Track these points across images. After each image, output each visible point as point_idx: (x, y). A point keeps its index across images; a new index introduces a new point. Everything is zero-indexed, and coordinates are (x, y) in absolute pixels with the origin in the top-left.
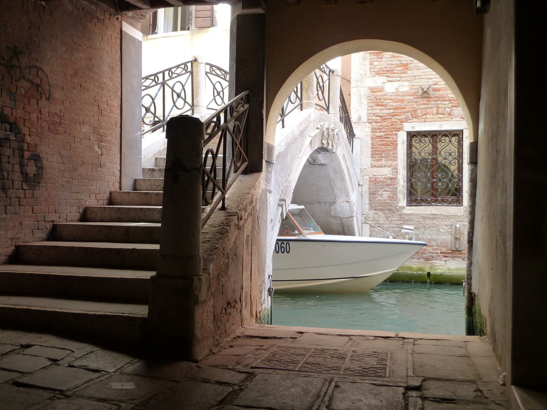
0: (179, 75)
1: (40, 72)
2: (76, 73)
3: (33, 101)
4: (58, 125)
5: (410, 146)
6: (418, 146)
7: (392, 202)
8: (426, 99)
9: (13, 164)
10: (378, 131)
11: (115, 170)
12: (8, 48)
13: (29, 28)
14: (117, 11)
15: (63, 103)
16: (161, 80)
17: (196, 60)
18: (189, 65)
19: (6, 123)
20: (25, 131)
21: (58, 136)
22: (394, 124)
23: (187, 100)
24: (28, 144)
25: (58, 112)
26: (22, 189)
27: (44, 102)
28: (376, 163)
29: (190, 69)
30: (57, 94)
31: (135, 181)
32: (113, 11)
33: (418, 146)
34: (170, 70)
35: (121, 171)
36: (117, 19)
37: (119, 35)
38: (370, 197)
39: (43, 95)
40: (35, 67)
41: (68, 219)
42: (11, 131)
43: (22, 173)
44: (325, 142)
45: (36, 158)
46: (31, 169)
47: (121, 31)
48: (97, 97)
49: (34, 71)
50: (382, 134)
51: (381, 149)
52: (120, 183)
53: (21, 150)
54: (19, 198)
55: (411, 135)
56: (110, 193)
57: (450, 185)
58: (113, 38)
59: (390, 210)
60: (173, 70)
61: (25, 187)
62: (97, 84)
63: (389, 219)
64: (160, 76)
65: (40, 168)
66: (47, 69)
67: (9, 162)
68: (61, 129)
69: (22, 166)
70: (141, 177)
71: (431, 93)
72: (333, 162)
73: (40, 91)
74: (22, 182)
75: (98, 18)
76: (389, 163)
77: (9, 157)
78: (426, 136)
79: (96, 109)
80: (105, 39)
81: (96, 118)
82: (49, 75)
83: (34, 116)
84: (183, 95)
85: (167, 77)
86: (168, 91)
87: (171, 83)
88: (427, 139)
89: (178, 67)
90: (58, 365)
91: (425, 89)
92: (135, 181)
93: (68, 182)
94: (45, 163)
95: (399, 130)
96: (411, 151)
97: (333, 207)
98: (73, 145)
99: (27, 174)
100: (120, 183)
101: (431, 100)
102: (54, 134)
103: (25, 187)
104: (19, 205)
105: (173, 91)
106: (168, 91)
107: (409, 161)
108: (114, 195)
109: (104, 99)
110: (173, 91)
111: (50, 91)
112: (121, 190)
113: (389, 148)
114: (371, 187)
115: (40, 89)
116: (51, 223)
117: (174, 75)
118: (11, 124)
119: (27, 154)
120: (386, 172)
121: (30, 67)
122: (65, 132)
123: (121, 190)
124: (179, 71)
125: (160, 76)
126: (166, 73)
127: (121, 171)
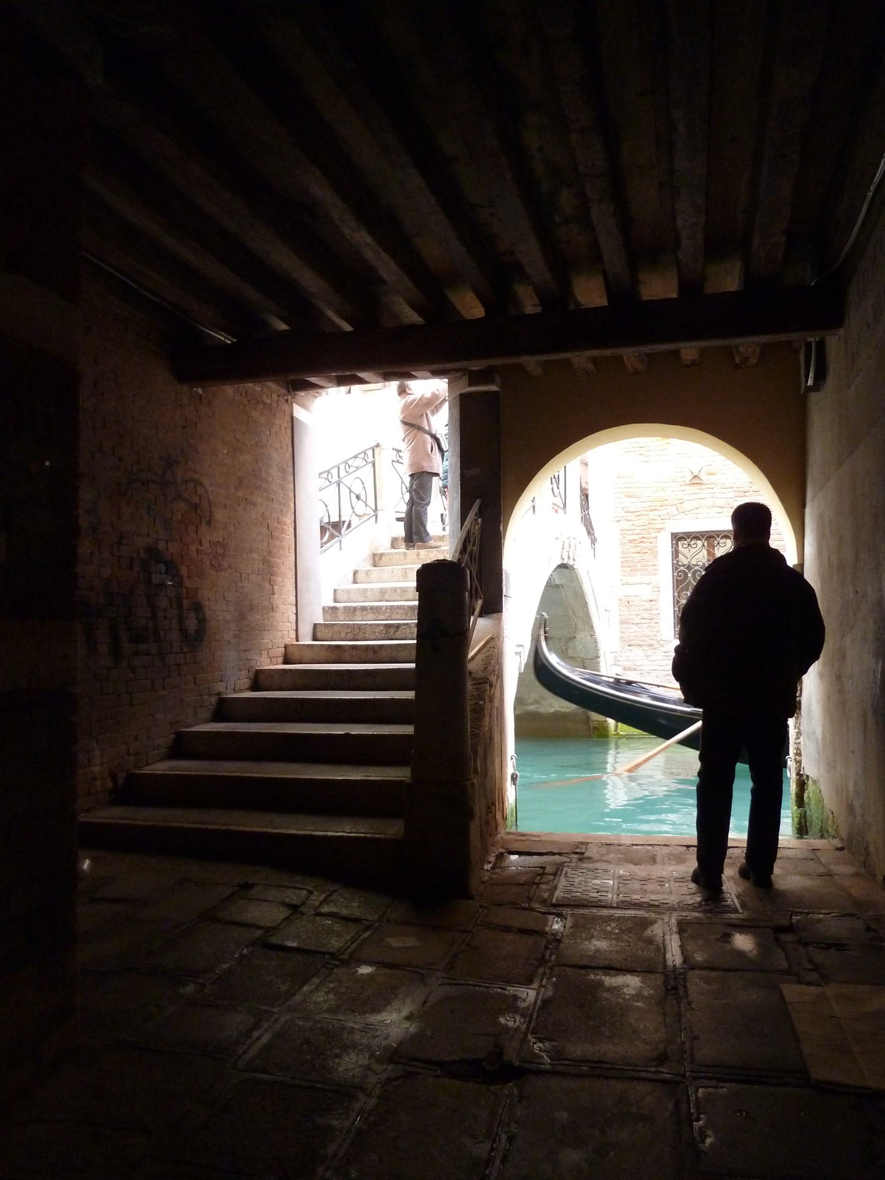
0: (358, 468)
1: (199, 487)
2: (241, 482)
3: (191, 529)
4: (220, 558)
5: (676, 553)
6: (685, 551)
7: (654, 633)
8: (697, 487)
9: (170, 619)
10: (629, 532)
11: (290, 613)
12: (160, 457)
13: (184, 427)
14: (289, 391)
15: (226, 527)
16: (336, 478)
17: (378, 446)
18: (370, 453)
19: (160, 562)
20: (184, 571)
21: (222, 573)
22: (652, 522)
23: (368, 503)
24: (187, 588)
25: (221, 540)
26: (182, 652)
27: (204, 528)
28: (631, 580)
29: (370, 459)
30: (219, 515)
31: (315, 625)
32: (283, 391)
33: (685, 551)
34: (346, 462)
35: (297, 614)
36: (287, 401)
37: (290, 424)
38: (621, 628)
39: (203, 519)
40: (192, 480)
41: (237, 689)
42: (167, 573)
43: (181, 629)
44: (565, 556)
45: (198, 607)
46: (191, 624)
47: (292, 417)
48: (267, 514)
49: (191, 485)
50: (636, 537)
51: (634, 562)
52: (297, 631)
53: (179, 598)
54: (179, 665)
55: (677, 538)
56: (285, 647)
57: (690, 575)
58: (283, 430)
59: (651, 645)
60: (350, 462)
61: (185, 649)
62: (266, 494)
63: (650, 658)
64: (334, 472)
65: (202, 621)
66: (206, 482)
67: (165, 617)
68: (225, 564)
69: (181, 620)
70: (322, 622)
71: (703, 476)
72: (572, 582)
73: (199, 513)
74: (182, 642)
75: (264, 404)
76: (647, 579)
77: (165, 610)
78: (697, 538)
79: (265, 530)
80: (273, 430)
81: (266, 544)
82: (210, 489)
83: (193, 548)
84: (363, 497)
85: (343, 473)
86: (344, 491)
87: (347, 480)
88: (699, 543)
89: (356, 457)
90: (303, 914)
91: (696, 473)
92: (315, 625)
93: (235, 636)
94: (208, 613)
95: (659, 530)
96: (678, 561)
97: (571, 644)
98: (240, 584)
99: (187, 632)
100: (297, 631)
101: (703, 487)
102: (217, 571)
103: (185, 649)
104: (180, 675)
105: (365, 503)
106: (344, 491)
107: (676, 574)
108: (290, 649)
109: (275, 515)
110: (365, 503)
111: (211, 512)
112: (297, 641)
113: (646, 557)
114: (622, 613)
115: (198, 510)
116: (216, 697)
117: (352, 469)
118: (165, 563)
119: (186, 603)
120: (646, 592)
121: (186, 482)
122: (230, 567)
123: (297, 641)
124: (359, 462)
125: (334, 472)
126: (342, 467)
127: (297, 614)
